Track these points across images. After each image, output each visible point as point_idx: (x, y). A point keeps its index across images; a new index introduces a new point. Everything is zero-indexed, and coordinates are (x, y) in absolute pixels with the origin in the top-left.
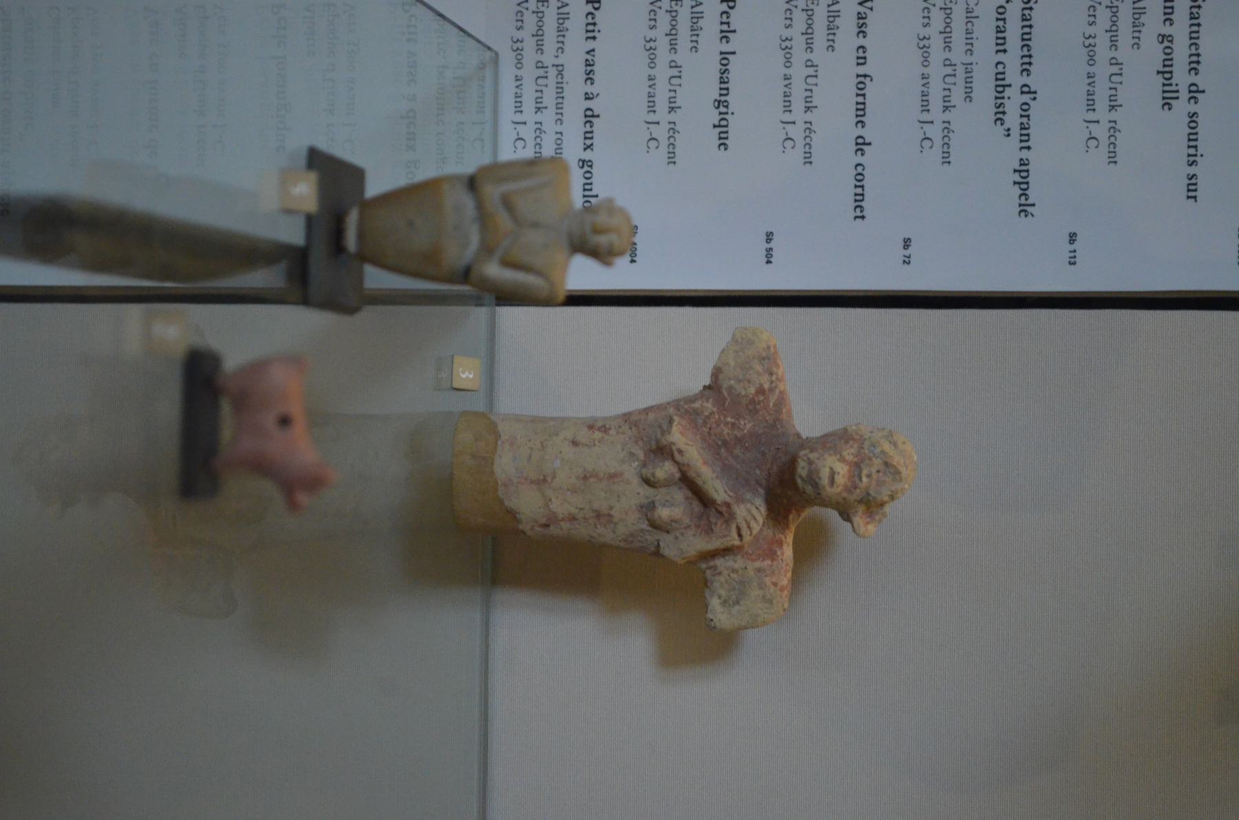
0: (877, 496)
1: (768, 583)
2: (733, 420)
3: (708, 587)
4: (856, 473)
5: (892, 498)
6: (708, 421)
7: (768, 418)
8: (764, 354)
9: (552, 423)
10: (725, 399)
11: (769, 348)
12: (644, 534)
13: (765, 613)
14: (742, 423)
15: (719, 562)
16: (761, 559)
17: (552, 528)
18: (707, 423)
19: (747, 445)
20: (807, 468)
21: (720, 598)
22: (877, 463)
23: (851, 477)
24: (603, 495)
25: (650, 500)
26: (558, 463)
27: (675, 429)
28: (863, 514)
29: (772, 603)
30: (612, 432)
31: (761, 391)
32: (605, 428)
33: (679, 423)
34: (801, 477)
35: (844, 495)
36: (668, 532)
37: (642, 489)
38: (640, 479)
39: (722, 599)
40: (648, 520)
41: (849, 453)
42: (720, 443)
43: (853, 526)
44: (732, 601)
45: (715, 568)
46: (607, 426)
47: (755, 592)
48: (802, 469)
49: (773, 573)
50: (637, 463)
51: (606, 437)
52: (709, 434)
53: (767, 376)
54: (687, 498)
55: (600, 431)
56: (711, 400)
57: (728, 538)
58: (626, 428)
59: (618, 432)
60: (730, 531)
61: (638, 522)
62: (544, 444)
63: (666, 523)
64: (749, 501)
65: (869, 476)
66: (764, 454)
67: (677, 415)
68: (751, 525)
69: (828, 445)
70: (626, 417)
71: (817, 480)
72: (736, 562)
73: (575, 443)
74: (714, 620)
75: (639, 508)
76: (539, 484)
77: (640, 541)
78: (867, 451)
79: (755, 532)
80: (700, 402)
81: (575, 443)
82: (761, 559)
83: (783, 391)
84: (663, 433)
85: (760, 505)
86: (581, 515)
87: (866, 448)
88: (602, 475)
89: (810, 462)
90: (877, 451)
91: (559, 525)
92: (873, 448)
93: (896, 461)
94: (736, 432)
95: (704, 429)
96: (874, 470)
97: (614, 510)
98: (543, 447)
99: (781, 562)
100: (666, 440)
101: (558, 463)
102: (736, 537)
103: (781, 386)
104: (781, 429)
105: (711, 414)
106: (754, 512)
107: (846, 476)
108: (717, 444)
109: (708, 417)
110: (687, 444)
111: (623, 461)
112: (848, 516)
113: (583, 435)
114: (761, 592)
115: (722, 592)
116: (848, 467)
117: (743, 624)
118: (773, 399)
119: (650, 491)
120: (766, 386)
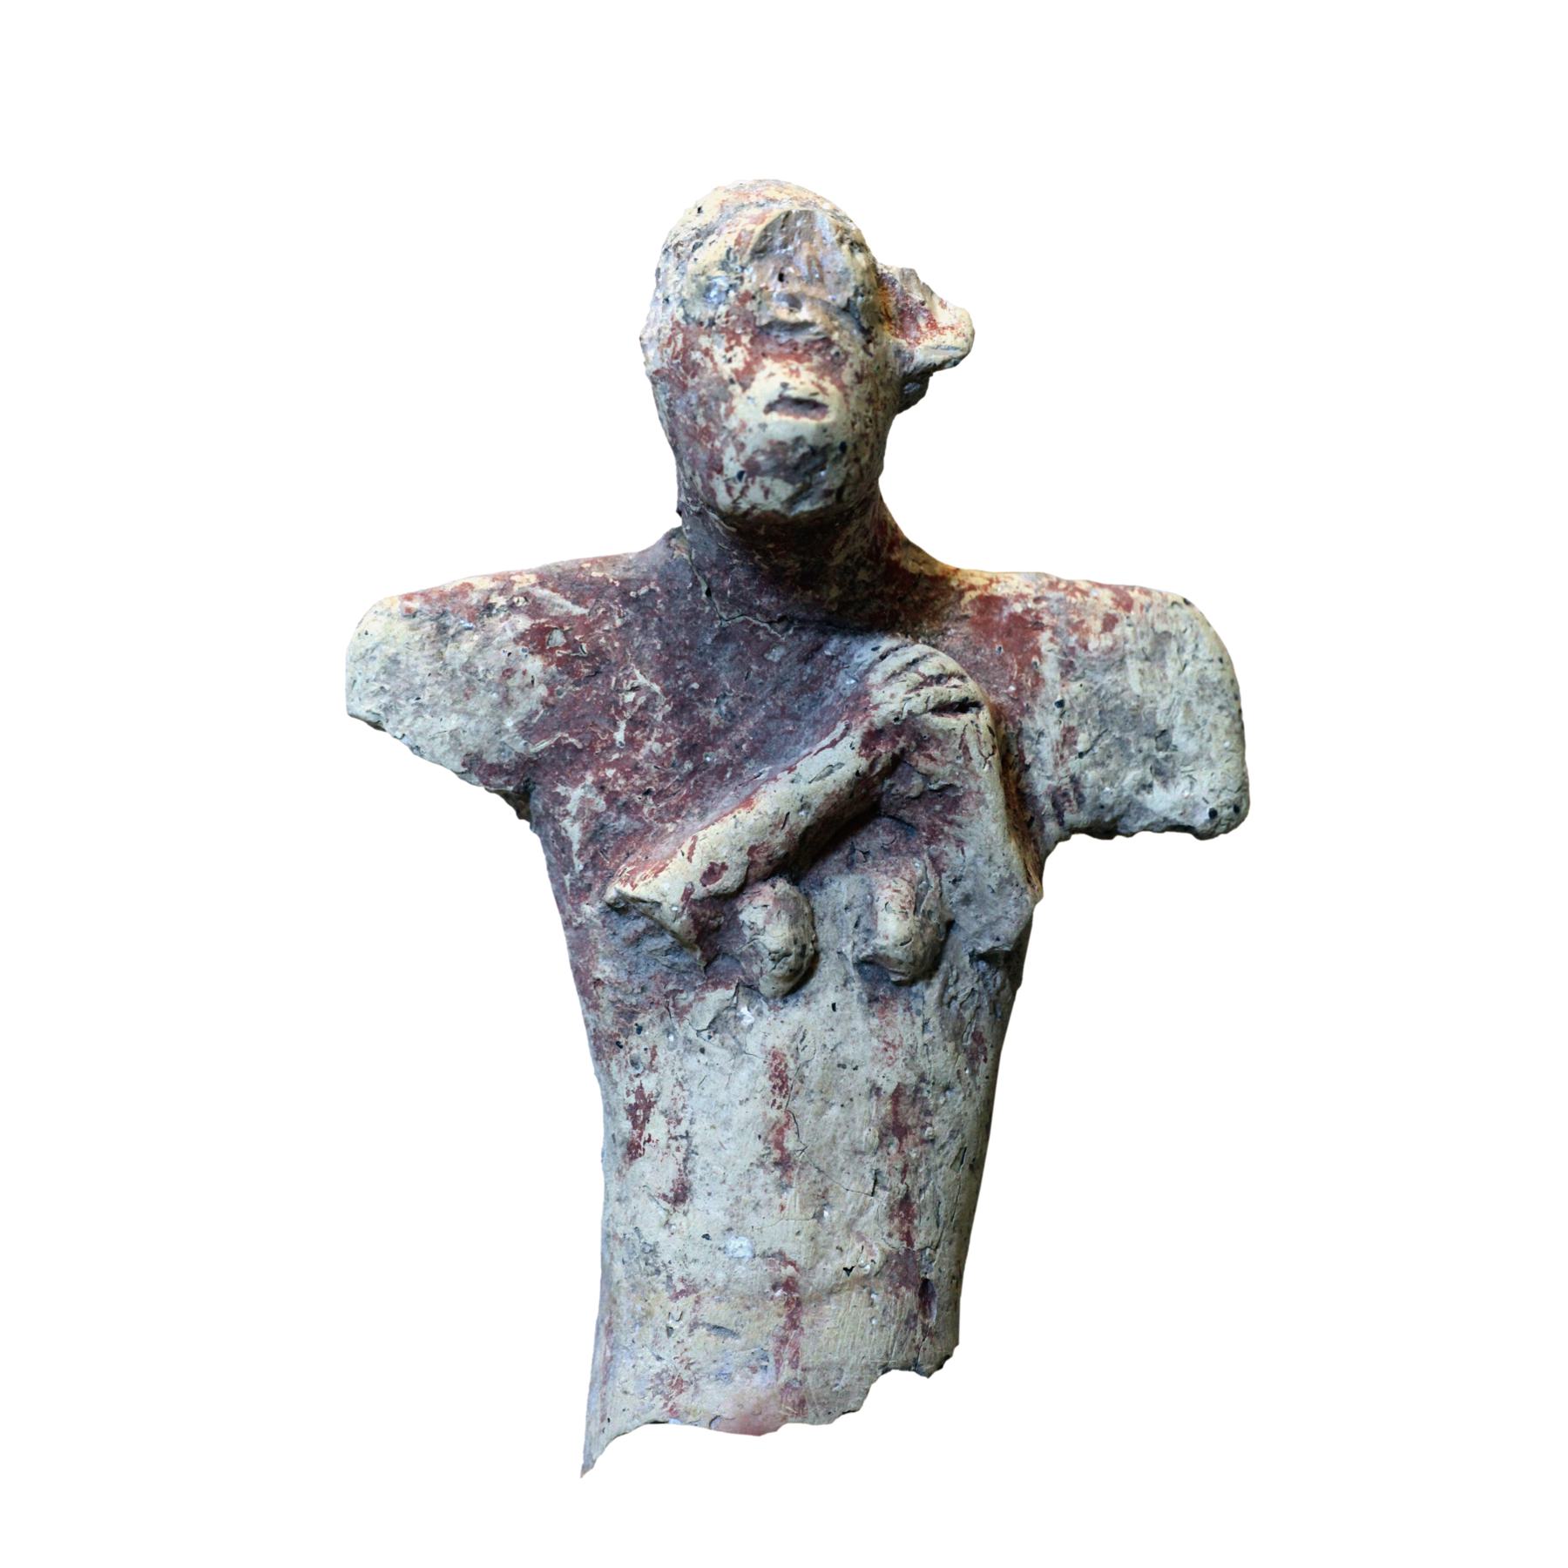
0: (853, 284)
1: (1107, 641)
2: (623, 725)
3: (1115, 820)
4: (784, 338)
5: (858, 245)
6: (623, 798)
7: (619, 622)
8: (429, 628)
9: (619, 1270)
10: (557, 743)
11: (410, 614)
12: (955, 998)
13: (1194, 657)
14: (630, 697)
15: (1042, 782)
16: (1035, 659)
17: (931, 1276)
18: (630, 800)
19: (695, 686)
20: (767, 481)
21: (1148, 787)
22: (752, 278)
23: (796, 353)
24: (834, 1112)
25: (853, 973)
26: (739, 1245)
27: (643, 889)
28: (905, 336)
29: (1167, 635)
30: (649, 1084)
31: (537, 640)
32: (636, 1107)
33: (629, 880)
34: (793, 501)
35: (847, 376)
36: (950, 925)
37: (820, 996)
38: (792, 1001)
39: (1150, 778)
40: (913, 982)
41: (725, 358)
42: (688, 766)
43: (941, 367)
44: (1159, 749)
45: (1058, 798)
46: (632, 1100)
47: (1133, 679)
48: (770, 495)
49: (1076, 627)
50: (744, 1010)
51: (663, 1103)
52: (660, 795)
53: (493, 620)
54: (850, 865)
55: (646, 1119)
56: (560, 789)
57: (970, 738)
58: (637, 1045)
59: (652, 1068)
60: (949, 733)
61: (919, 1013)
62: (680, 1287)
63: (923, 926)
64: (861, 678)
65: (794, 302)
66: (723, 637)
67: (601, 894)
68: (934, 672)
69: (701, 421)
70: (604, 1046)
71: (802, 451)
72: (1041, 734)
73: (680, 1195)
74: (1213, 805)
75: (877, 1006)
76: (799, 1303)
77: (976, 1015)
78: (723, 309)
79: (952, 666)
80: (566, 823)
81: (680, 1195)
82: (1035, 659)
83: (539, 576)
84: (659, 928)
85: (874, 649)
86: (894, 1181)
87: (711, 313)
88: (774, 1114)
89: (751, 470)
90: (722, 281)
91: (922, 1250)
92: (713, 293)
93: (750, 228)
94: (659, 717)
95: (646, 810)
96: (777, 288)
97: (880, 1082)
98: (690, 1289)
99: (1044, 604)
100: (678, 916)
101: (739, 1245)
102: (969, 716)
103: (525, 582)
104: (652, 585)
105: (602, 789)
106: (893, 663)
107: (794, 365)
108: (692, 774)
109: (612, 799)
110: (691, 853)
111: (739, 1051)
112: (907, 378)
113: (657, 1171)
114: (1133, 665)
115: (1131, 777)
116: (767, 362)
117: (1227, 722)
118: (563, 605)
119: (827, 970)
120: (523, 623)
